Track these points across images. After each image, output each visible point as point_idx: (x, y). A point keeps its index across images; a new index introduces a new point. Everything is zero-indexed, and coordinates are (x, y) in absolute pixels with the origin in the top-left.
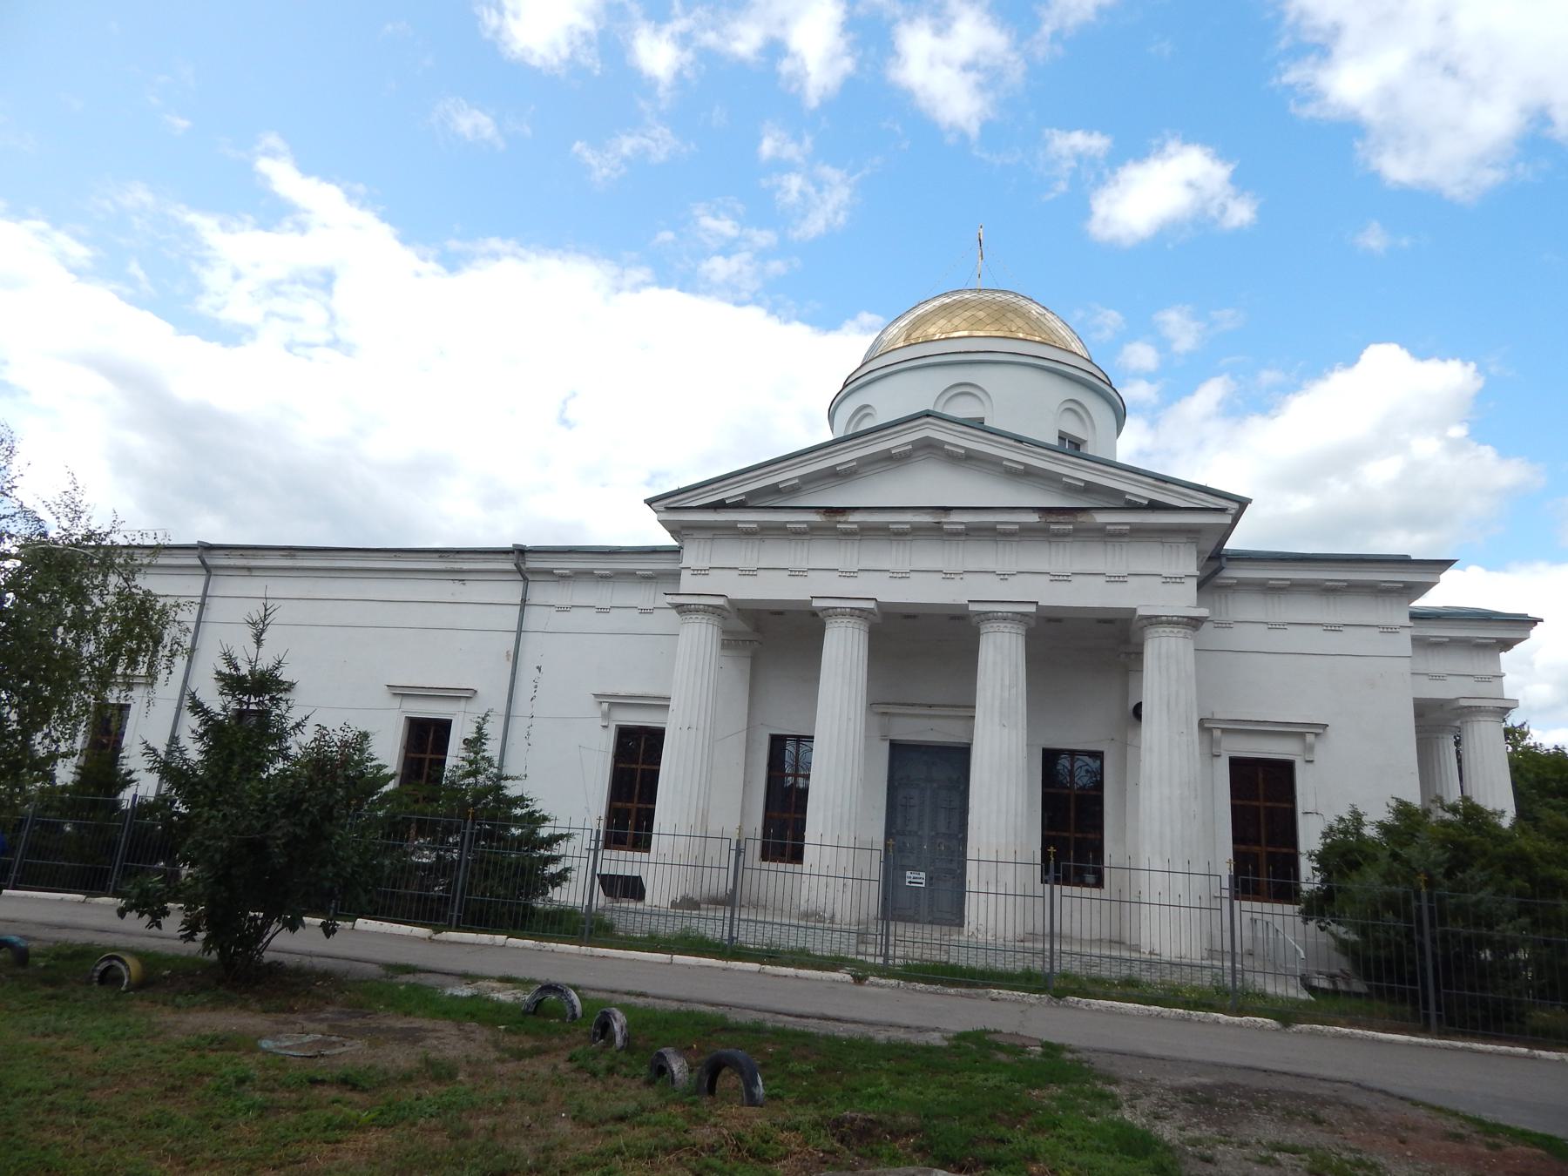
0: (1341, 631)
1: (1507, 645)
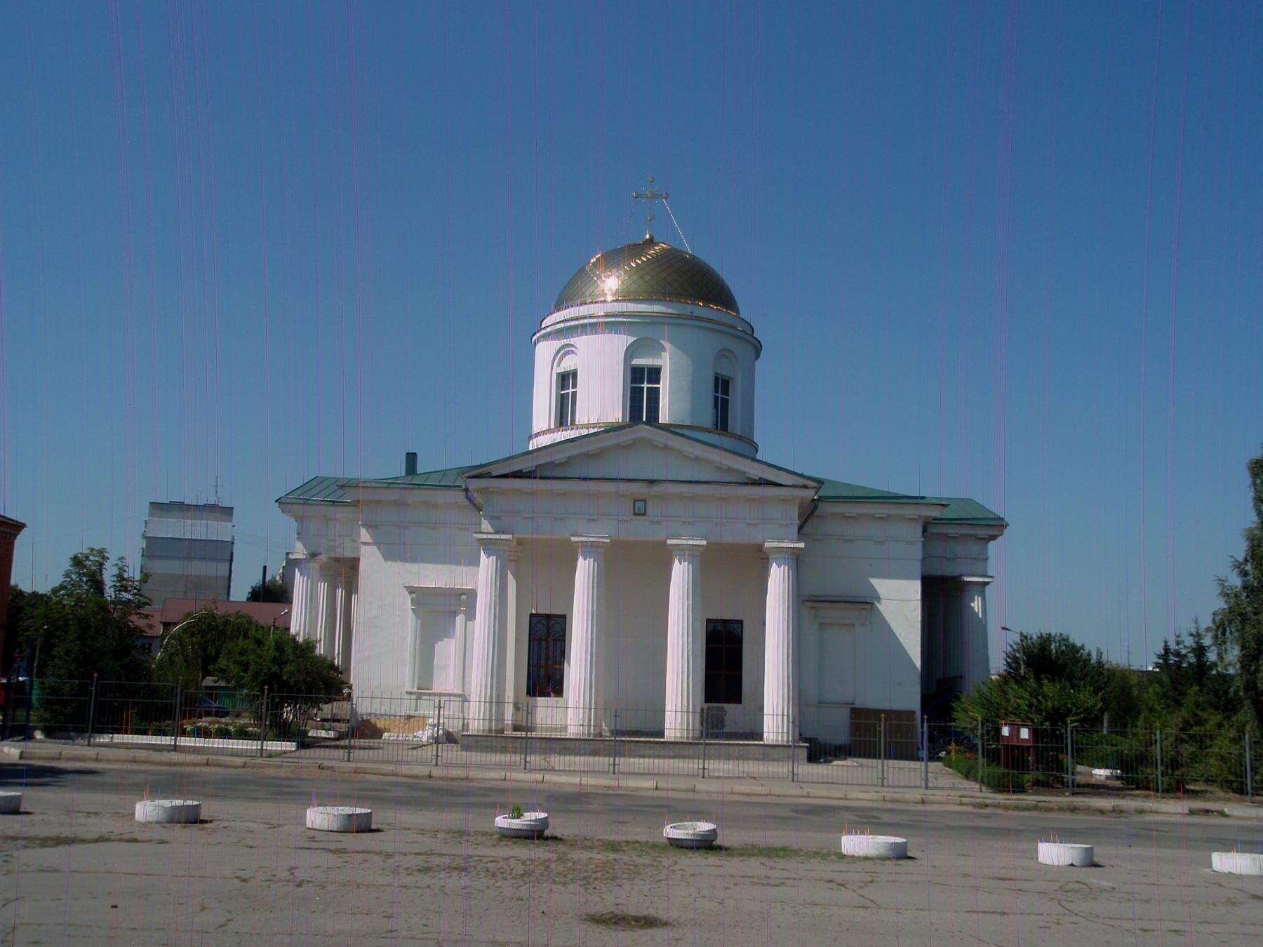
1: (993, 538)
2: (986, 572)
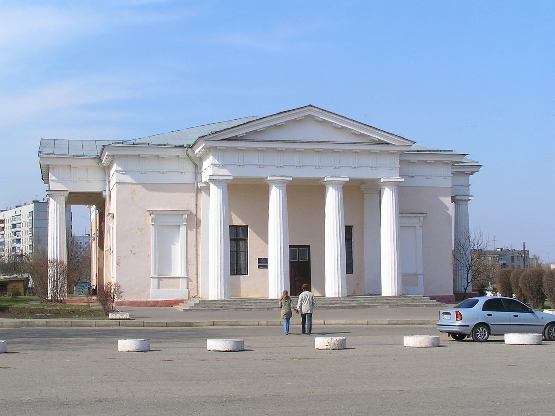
0: (283, 168)
1: (472, 173)
2: (469, 194)
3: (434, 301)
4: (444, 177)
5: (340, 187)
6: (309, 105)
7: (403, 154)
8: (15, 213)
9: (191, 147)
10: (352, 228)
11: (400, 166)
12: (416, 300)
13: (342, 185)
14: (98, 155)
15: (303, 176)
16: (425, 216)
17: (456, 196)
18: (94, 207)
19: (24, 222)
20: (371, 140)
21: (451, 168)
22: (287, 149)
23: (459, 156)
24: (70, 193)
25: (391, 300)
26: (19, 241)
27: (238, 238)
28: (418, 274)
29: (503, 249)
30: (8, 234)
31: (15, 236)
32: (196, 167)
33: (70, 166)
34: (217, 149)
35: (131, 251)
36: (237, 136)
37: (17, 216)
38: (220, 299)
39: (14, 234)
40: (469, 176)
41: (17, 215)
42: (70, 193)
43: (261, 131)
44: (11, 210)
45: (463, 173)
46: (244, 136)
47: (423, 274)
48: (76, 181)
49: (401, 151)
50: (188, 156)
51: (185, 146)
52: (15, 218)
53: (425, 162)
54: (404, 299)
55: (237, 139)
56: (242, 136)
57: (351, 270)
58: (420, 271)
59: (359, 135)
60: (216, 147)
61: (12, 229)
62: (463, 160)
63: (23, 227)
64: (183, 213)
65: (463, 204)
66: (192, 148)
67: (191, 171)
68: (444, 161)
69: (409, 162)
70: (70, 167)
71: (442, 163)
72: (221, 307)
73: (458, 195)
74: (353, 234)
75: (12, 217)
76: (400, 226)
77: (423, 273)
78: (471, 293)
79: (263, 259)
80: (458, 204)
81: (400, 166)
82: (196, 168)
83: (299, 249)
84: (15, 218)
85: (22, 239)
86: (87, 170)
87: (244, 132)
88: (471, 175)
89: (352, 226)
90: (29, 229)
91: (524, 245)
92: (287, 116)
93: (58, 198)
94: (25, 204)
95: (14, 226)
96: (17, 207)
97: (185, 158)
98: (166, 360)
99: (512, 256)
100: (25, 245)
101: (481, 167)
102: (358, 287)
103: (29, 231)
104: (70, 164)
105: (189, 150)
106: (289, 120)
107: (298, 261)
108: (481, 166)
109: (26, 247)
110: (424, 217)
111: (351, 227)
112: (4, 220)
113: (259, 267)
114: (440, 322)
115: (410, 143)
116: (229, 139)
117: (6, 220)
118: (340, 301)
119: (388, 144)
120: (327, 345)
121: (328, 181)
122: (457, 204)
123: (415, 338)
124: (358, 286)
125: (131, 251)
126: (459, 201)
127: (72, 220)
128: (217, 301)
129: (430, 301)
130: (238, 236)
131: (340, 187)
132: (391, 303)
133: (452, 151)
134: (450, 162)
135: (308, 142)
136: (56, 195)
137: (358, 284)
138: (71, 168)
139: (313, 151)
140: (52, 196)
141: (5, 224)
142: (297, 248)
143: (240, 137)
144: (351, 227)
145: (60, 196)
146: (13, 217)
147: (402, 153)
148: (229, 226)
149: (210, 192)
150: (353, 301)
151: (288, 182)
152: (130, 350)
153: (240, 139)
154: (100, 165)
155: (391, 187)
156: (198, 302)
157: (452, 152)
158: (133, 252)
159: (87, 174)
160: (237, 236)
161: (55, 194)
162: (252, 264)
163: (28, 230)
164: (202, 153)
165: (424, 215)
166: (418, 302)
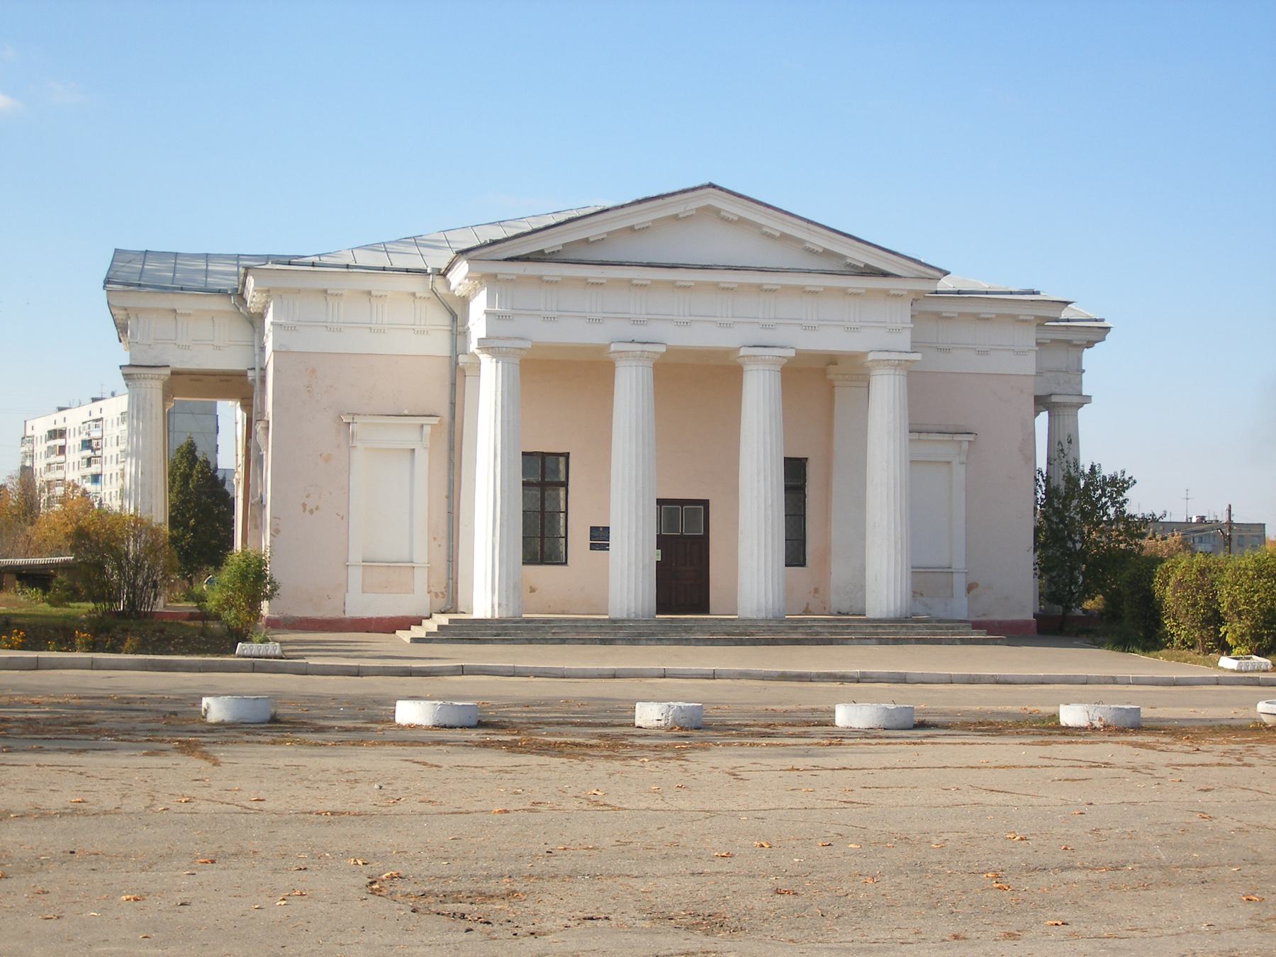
1: (1090, 344)
3: (981, 633)
4: (1018, 353)
5: (773, 370)
6: (707, 182)
7: (922, 297)
8: (90, 415)
9: (442, 275)
10: (807, 464)
11: (912, 326)
12: (941, 628)
13: (780, 367)
14: (237, 289)
15: (692, 344)
16: (973, 439)
17: (1051, 395)
18: (239, 403)
19: (108, 435)
20: (849, 265)
21: (1035, 329)
22: (656, 283)
23: (1054, 304)
24: (173, 373)
25: (883, 628)
26: (96, 478)
27: (546, 480)
28: (953, 571)
29: (1207, 519)
30: (74, 463)
31: (87, 467)
32: (454, 317)
33: (175, 311)
34: (499, 280)
35: (304, 505)
36: (542, 252)
37: (94, 420)
38: (497, 616)
39: (86, 463)
40: (1083, 350)
41: (94, 418)
42: (173, 373)
43: (598, 240)
44: (81, 408)
45: (1069, 343)
46: (558, 251)
47: (966, 571)
48: (189, 346)
49: (917, 292)
50: (436, 294)
51: (429, 271)
52: (89, 425)
53: (977, 318)
54: (913, 627)
55: (542, 257)
56: (553, 252)
57: (802, 559)
58: (959, 564)
59: (821, 253)
60: (495, 276)
61: (81, 450)
62: (1064, 315)
63: (106, 446)
64: (422, 423)
65: (1061, 414)
66: (444, 275)
67: (244, 343)
68: (1018, 315)
69: (938, 316)
70: (174, 315)
71: (1015, 319)
72: (498, 635)
73: (1056, 394)
74: (807, 477)
75: (83, 423)
76: (911, 461)
77: (966, 568)
78: (1082, 616)
79: (601, 529)
80: (1056, 414)
81: (912, 326)
82: (453, 321)
83: (684, 507)
84: (89, 425)
85: (103, 474)
86: (213, 321)
87: (558, 244)
88: (1087, 348)
89: (807, 459)
90: (121, 452)
91: (1230, 511)
92: (625, 215)
93: (146, 384)
94: (113, 395)
95: (87, 444)
96: (94, 400)
97: (429, 298)
98: (432, 766)
99: (1239, 536)
100: (111, 488)
101: (1109, 331)
102: (817, 598)
103: (119, 456)
104: (176, 307)
105: (439, 280)
106: (662, 215)
107: (682, 536)
108: (1109, 328)
109: (114, 494)
110: (969, 442)
111: (804, 461)
112: (66, 430)
113: (593, 547)
114: (274, 624)
115: (937, 274)
116: (525, 257)
117: (70, 430)
118: (767, 628)
119: (885, 274)
120: (658, 720)
121: (747, 356)
122: (1053, 414)
123: (858, 708)
124: (816, 595)
125: (304, 505)
126: (1058, 407)
127: (218, 432)
128: (490, 622)
129: (972, 632)
130: (546, 475)
131: (773, 370)
132: (883, 634)
133: (1038, 293)
134: (1033, 318)
135: (703, 268)
136: (142, 376)
137: (816, 591)
138: (177, 318)
139: (717, 287)
140: (134, 379)
141: (68, 440)
142: (680, 507)
143: (549, 253)
144: (804, 461)
145: (144, 378)
146: (85, 424)
147: (917, 298)
148: (568, 451)
149: (480, 376)
150: (797, 628)
151: (657, 357)
152: (225, 719)
153: (548, 257)
154: (241, 310)
155: (892, 373)
156: (447, 623)
157: (1037, 296)
158: (308, 508)
159: (214, 326)
160: (543, 476)
161: (140, 374)
162: (578, 539)
163: (117, 455)
164: (466, 288)
165: (971, 438)
166: (945, 633)
